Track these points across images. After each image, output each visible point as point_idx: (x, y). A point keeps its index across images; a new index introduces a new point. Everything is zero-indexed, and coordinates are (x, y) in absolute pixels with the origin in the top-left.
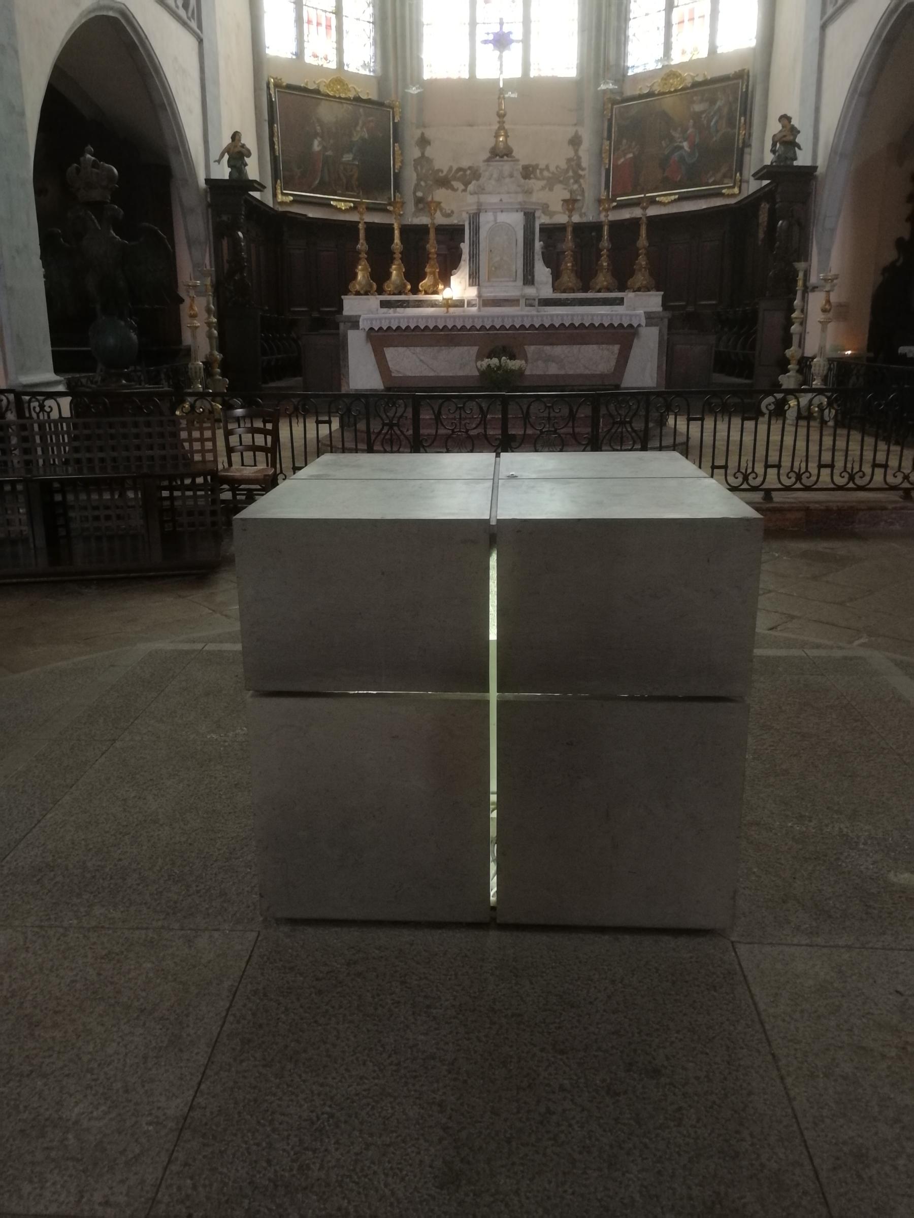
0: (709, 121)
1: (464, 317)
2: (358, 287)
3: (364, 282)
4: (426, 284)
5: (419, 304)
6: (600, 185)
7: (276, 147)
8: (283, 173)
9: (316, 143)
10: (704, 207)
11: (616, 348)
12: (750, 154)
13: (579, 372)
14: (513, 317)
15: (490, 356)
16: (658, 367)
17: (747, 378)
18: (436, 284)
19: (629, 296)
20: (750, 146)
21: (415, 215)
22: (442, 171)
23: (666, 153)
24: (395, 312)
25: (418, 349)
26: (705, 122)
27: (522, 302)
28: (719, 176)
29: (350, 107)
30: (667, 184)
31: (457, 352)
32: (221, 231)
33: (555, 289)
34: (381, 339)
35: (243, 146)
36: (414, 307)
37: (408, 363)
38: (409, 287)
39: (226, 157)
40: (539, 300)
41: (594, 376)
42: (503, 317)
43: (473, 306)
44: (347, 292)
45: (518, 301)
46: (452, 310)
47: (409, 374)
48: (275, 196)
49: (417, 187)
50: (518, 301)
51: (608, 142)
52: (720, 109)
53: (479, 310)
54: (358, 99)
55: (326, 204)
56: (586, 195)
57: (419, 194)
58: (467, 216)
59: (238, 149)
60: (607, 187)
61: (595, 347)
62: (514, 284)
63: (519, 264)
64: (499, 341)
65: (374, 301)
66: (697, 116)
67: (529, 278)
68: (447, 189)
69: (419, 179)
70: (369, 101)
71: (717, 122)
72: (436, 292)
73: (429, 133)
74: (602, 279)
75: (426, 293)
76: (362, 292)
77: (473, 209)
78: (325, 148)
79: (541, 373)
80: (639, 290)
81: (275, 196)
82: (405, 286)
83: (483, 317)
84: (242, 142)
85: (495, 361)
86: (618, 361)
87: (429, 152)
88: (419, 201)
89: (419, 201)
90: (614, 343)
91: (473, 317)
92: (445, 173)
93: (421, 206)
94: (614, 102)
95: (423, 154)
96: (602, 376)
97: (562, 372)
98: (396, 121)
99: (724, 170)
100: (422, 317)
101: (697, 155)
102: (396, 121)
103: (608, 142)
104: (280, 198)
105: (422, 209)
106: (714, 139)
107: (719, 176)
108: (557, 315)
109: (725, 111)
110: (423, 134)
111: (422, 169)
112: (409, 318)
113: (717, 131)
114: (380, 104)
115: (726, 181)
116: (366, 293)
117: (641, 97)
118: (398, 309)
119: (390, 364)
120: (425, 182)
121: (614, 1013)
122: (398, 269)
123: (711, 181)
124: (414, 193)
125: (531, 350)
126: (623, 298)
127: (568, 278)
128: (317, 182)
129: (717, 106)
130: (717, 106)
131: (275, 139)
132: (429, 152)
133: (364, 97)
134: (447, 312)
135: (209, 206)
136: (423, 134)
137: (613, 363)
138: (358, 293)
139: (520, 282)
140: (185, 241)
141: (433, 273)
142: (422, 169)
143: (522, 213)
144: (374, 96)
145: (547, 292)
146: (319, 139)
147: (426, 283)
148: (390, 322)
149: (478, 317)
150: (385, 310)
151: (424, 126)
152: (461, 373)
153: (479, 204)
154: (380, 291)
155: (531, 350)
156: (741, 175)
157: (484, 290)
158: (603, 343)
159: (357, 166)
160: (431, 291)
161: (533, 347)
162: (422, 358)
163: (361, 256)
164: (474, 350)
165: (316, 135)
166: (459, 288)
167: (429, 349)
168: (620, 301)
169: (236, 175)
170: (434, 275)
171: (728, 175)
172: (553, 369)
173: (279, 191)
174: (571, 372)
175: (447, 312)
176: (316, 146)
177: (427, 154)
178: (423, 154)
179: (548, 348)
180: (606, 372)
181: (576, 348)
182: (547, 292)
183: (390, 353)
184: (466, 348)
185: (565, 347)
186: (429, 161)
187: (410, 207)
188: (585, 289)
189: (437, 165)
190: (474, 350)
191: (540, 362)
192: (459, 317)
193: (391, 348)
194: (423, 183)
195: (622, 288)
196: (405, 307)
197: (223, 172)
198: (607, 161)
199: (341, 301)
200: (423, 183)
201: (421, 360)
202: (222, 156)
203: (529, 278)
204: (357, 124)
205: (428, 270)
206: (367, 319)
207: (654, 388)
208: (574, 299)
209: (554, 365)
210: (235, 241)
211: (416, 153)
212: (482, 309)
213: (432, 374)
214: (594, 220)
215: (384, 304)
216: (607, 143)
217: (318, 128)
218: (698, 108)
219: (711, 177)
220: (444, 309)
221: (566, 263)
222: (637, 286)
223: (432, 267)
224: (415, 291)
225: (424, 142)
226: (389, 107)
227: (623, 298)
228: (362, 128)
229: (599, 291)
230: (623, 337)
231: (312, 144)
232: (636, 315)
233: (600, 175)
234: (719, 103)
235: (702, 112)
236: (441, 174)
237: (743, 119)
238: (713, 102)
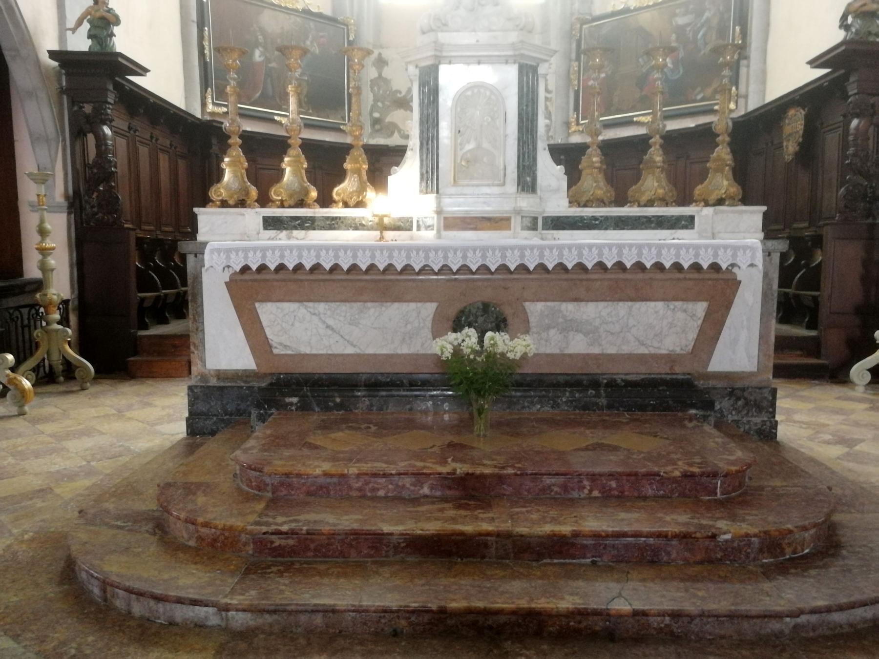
0: (696, 33)
1: (409, 250)
2: (224, 194)
3: (236, 186)
4: (344, 190)
5: (333, 224)
6: (568, 103)
7: (207, 52)
8: (209, 78)
9: (257, 53)
10: (693, 125)
11: (701, 308)
12: (748, 66)
13: (626, 349)
14: (504, 249)
15: (457, 327)
16: (761, 337)
17: (808, 327)
18: (362, 190)
19: (703, 214)
20: (747, 58)
21: (371, 136)
22: (400, 92)
23: (644, 71)
24: (289, 238)
25: (322, 307)
26: (691, 35)
27: (516, 222)
28: (709, 91)
29: (298, 19)
30: (645, 102)
31: (395, 314)
32: (82, 127)
33: (574, 201)
34: (253, 285)
35: (110, 11)
36: (323, 228)
37: (308, 333)
38: (314, 194)
39: (86, 26)
40: (545, 219)
41: (656, 357)
42: (484, 250)
43: (428, 227)
44: (205, 201)
45: (508, 219)
46: (389, 235)
47: (306, 350)
48: (204, 105)
49: (374, 108)
50: (508, 219)
51: (576, 64)
52: (708, 20)
53: (439, 236)
54: (307, 12)
55: (269, 119)
56: (553, 118)
57: (376, 115)
58: (417, 72)
59: (102, 13)
60: (576, 109)
61: (660, 305)
62: (496, 190)
63: (509, 155)
64: (481, 300)
65: (253, 216)
66: (680, 31)
67: (527, 179)
68: (406, 110)
69: (376, 100)
70: (320, 15)
71: (704, 35)
72: (360, 204)
73: (386, 54)
74: (653, 183)
75: (346, 205)
76: (231, 202)
77: (425, 58)
78: (268, 60)
79: (556, 351)
80: (720, 202)
81: (204, 105)
82: (307, 193)
83: (445, 250)
84: (110, 6)
85: (469, 338)
86: (702, 332)
87: (387, 72)
88: (375, 122)
89: (375, 122)
90: (696, 299)
91: (426, 249)
92: (403, 94)
93: (377, 127)
94: (584, 22)
95: (380, 75)
96: (671, 358)
97: (596, 350)
98: (351, 39)
99: (715, 85)
100: (345, 248)
101: (681, 72)
102: (351, 39)
103: (576, 64)
104: (210, 108)
105: (377, 131)
106: (702, 52)
107: (709, 91)
108: (590, 247)
109: (715, 22)
110: (380, 54)
111: (379, 89)
112: (319, 248)
113: (706, 44)
114: (332, 20)
115: (717, 97)
116: (242, 204)
117: (614, 14)
118: (295, 233)
119: (268, 332)
120: (383, 103)
121: (471, 405)
122: (295, 163)
123: (699, 97)
124: (371, 114)
125: (536, 309)
126: (692, 218)
127: (593, 182)
128: (258, 95)
129: (705, 18)
130: (705, 18)
131: (206, 43)
132: (387, 72)
133: (314, 10)
134: (382, 238)
135: (62, 91)
136: (380, 54)
137: (692, 335)
138: (224, 204)
139: (511, 187)
140: (28, 136)
141: (358, 171)
142: (379, 89)
143: (516, 67)
144: (327, 11)
145: (558, 204)
146: (261, 49)
147: (345, 188)
148: (264, 256)
149: (436, 249)
150: (272, 233)
151: (381, 47)
152: (405, 350)
153: (438, 47)
154: (264, 201)
155: (536, 309)
156: (737, 89)
157: (446, 201)
158: (676, 299)
159: (307, 81)
160: (352, 202)
161: (540, 306)
162: (330, 322)
163: (230, 141)
164: (429, 309)
165: (257, 45)
166: (403, 194)
167: (344, 307)
168: (688, 222)
169: (97, 49)
170: (360, 176)
171: (724, 91)
172: (578, 345)
173: (210, 100)
174: (612, 350)
175: (382, 238)
176: (258, 56)
177: (384, 75)
178: (380, 75)
179: (569, 308)
180: (678, 350)
181: (622, 308)
182: (558, 204)
183: (269, 313)
184: (413, 305)
185: (601, 305)
186: (387, 81)
187: (368, 129)
188: (620, 201)
189: (395, 86)
190: (429, 309)
191: (552, 332)
192: (400, 248)
193: (269, 304)
194: (380, 104)
195: (685, 199)
196: (308, 228)
197: (80, 43)
198: (576, 82)
199: (194, 217)
200: (380, 104)
201: (328, 327)
202: (79, 23)
203: (527, 179)
204: (307, 38)
205: (347, 165)
206: (219, 251)
207: (751, 374)
208: (607, 218)
209: (580, 337)
210: (101, 140)
211: (373, 73)
212: (444, 233)
213: (350, 350)
214: (563, 142)
215: (271, 223)
216: (575, 64)
217: (260, 37)
218: (681, 21)
219: (700, 92)
220: (377, 233)
221: (590, 157)
222: (713, 198)
223: (356, 161)
224: (326, 201)
225: (381, 62)
226: (344, 24)
227: (692, 218)
228: (312, 42)
229: (650, 203)
230: (712, 285)
231: (252, 54)
232: (745, 248)
233: (568, 97)
234: (707, 14)
235: (688, 25)
236: (398, 95)
237: (738, 28)
238: (699, 13)
